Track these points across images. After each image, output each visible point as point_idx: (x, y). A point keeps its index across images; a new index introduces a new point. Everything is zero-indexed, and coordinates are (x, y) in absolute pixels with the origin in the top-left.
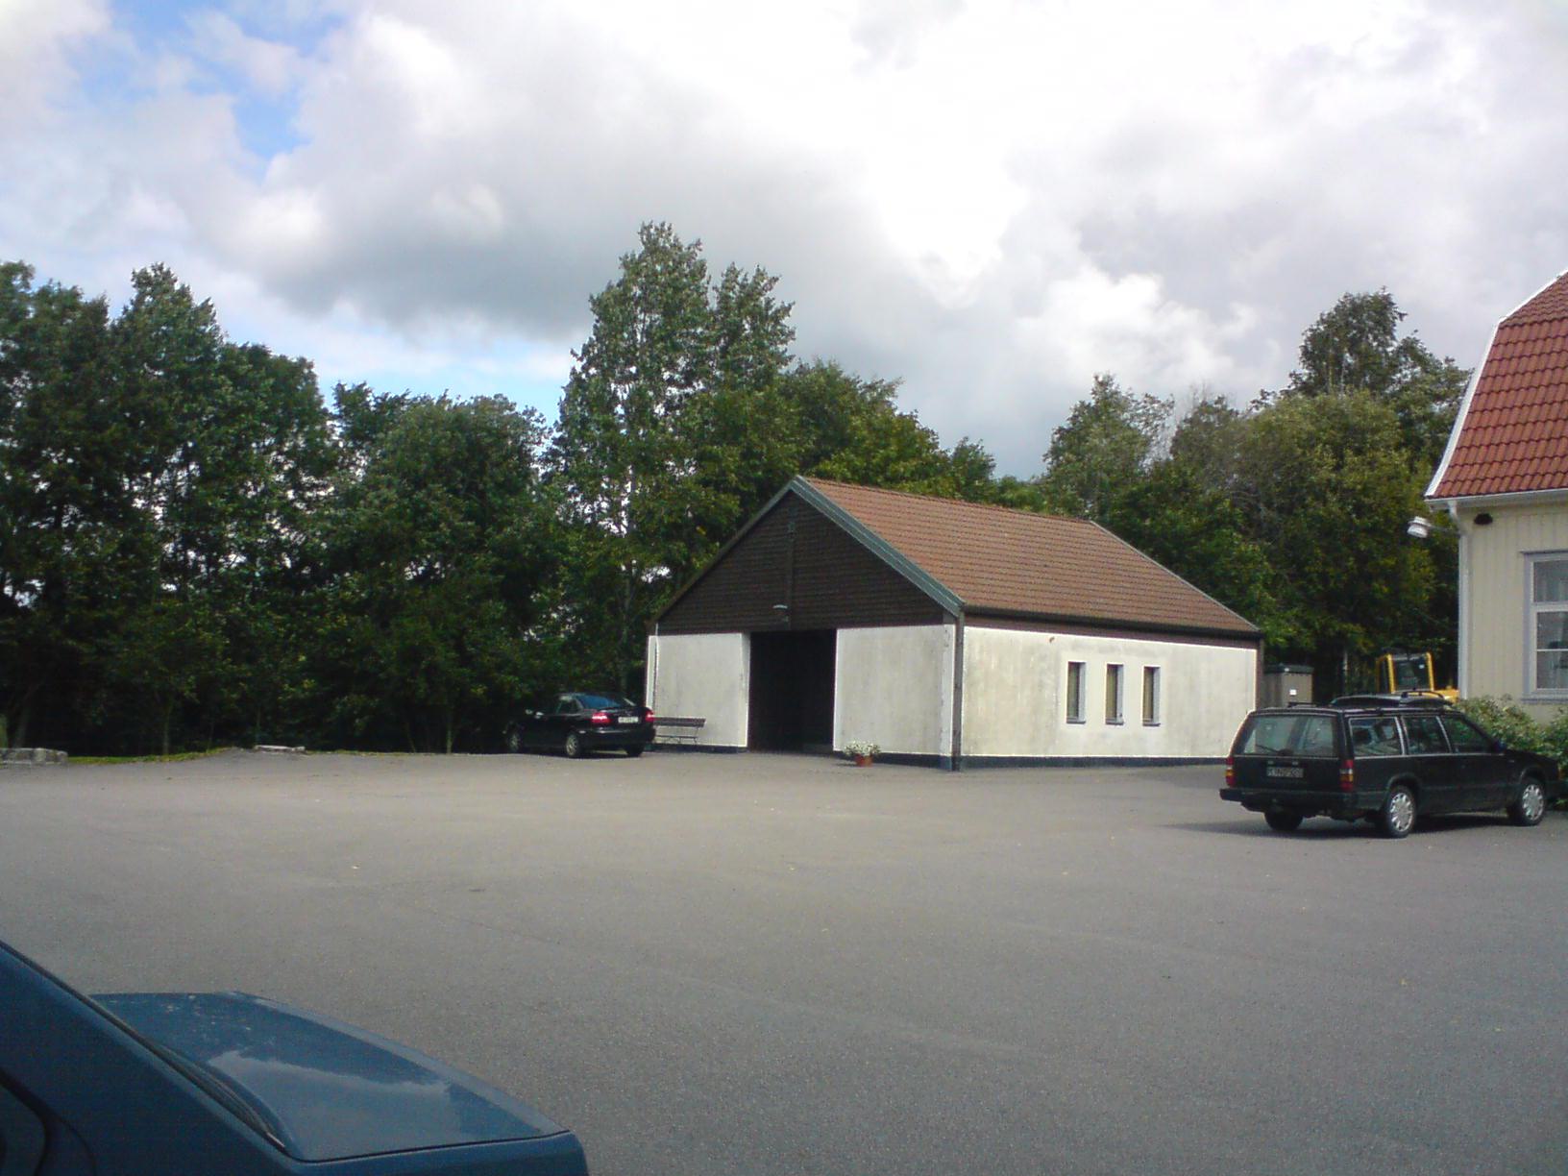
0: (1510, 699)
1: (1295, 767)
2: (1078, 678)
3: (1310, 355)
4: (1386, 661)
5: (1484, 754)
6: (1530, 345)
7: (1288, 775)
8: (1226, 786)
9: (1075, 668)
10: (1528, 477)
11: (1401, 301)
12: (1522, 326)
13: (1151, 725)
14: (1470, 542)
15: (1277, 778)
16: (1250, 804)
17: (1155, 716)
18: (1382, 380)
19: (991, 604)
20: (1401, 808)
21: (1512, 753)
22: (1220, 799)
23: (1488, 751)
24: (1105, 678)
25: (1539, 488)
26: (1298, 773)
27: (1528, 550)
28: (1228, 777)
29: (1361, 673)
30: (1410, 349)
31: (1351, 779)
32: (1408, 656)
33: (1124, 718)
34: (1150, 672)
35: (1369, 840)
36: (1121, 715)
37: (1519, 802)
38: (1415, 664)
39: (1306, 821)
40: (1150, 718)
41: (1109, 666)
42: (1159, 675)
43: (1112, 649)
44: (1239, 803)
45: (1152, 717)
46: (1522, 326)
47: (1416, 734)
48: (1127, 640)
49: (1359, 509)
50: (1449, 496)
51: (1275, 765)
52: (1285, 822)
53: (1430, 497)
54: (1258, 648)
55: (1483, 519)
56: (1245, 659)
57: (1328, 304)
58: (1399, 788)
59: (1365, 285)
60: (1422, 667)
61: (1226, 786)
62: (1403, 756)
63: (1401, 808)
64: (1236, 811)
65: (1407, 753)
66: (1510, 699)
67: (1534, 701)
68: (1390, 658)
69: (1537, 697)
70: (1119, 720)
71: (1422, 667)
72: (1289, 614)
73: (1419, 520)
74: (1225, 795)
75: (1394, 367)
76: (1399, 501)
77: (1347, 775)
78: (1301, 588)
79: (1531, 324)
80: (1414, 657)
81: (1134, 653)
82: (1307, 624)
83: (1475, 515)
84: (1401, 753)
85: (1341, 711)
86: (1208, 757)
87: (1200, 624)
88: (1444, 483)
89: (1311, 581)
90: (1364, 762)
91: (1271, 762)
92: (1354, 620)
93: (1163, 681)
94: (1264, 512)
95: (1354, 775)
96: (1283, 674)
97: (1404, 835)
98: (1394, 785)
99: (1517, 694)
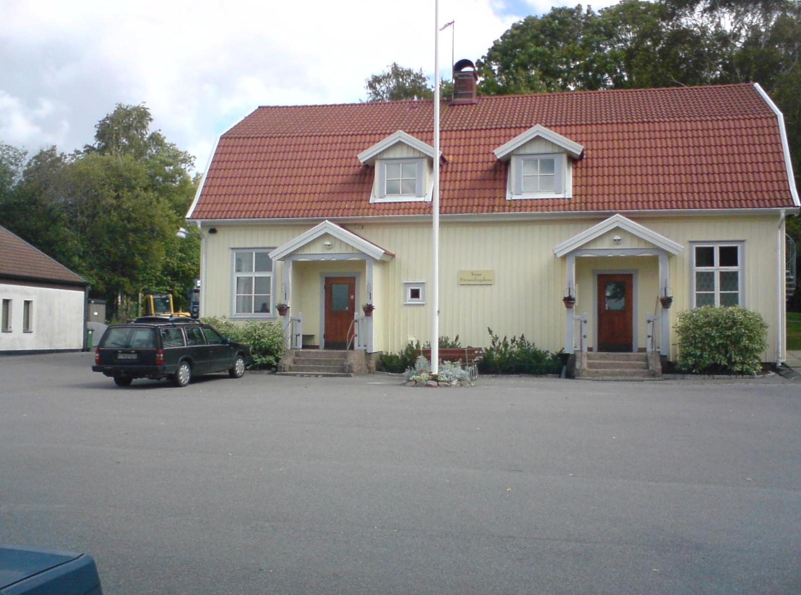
0: (225, 318)
1: (133, 353)
2: (8, 307)
3: (100, 136)
4: (150, 298)
5: (219, 345)
6: (234, 148)
7: (129, 358)
8: (95, 364)
9: (359, 346)
10: (225, 213)
11: (153, 112)
12: (257, 138)
13: (28, 332)
14: (206, 241)
15: (122, 359)
16: (108, 373)
17: (30, 327)
18: (140, 153)
19: (34, 275)
20: (184, 372)
21: (231, 344)
22: (92, 371)
23: (221, 343)
24: (23, 309)
25: (240, 218)
26: (134, 357)
27: (233, 247)
28: (96, 360)
29: (128, 303)
30: (156, 139)
31: (162, 359)
32: (161, 296)
33: (13, 329)
34: (27, 303)
35: (171, 389)
36: (11, 327)
37: (234, 367)
38: (164, 300)
39: (135, 381)
40: (27, 328)
41: (25, 301)
42: (32, 305)
43: (6, 291)
44: (102, 373)
45: (28, 328)
46: (257, 138)
47: (191, 336)
48: (15, 286)
49: (129, 219)
50: (197, 218)
51: (122, 353)
52: (123, 382)
53: (188, 219)
54: (85, 291)
55: (213, 231)
56: (78, 297)
57: (110, 110)
58: (185, 362)
59: (132, 101)
60: (167, 301)
61: (95, 364)
62: (185, 347)
63: (184, 372)
64: (101, 377)
65: (187, 345)
66: (225, 318)
67: (235, 319)
68: (151, 297)
69: (236, 317)
70: (9, 330)
71: (167, 301)
72: (92, 272)
73: (182, 229)
74: (95, 369)
75: (146, 146)
76: (150, 217)
77: (160, 357)
78: (98, 258)
79: (235, 138)
80: (164, 297)
81: (33, 292)
82: (102, 278)
83: (209, 229)
84: (184, 345)
85: (156, 325)
86: (59, 348)
87: (54, 277)
88: (194, 212)
89: (103, 255)
90: (168, 351)
91: (120, 351)
92: (124, 275)
93: (34, 308)
94: (79, 218)
95: (163, 357)
96: (91, 304)
97: (185, 386)
98: (183, 360)
99: (228, 315)
